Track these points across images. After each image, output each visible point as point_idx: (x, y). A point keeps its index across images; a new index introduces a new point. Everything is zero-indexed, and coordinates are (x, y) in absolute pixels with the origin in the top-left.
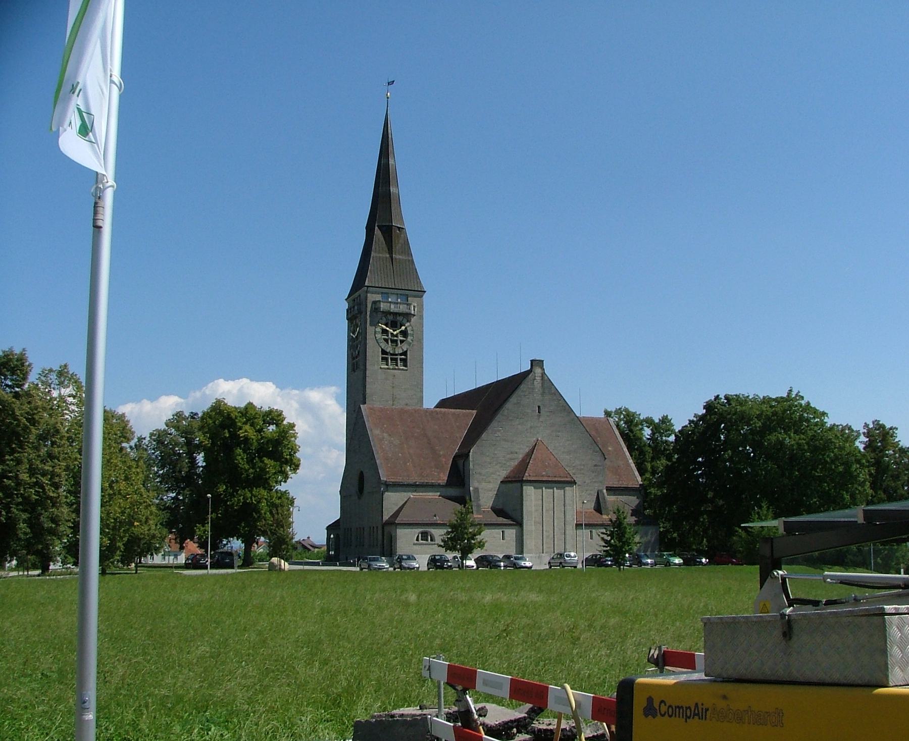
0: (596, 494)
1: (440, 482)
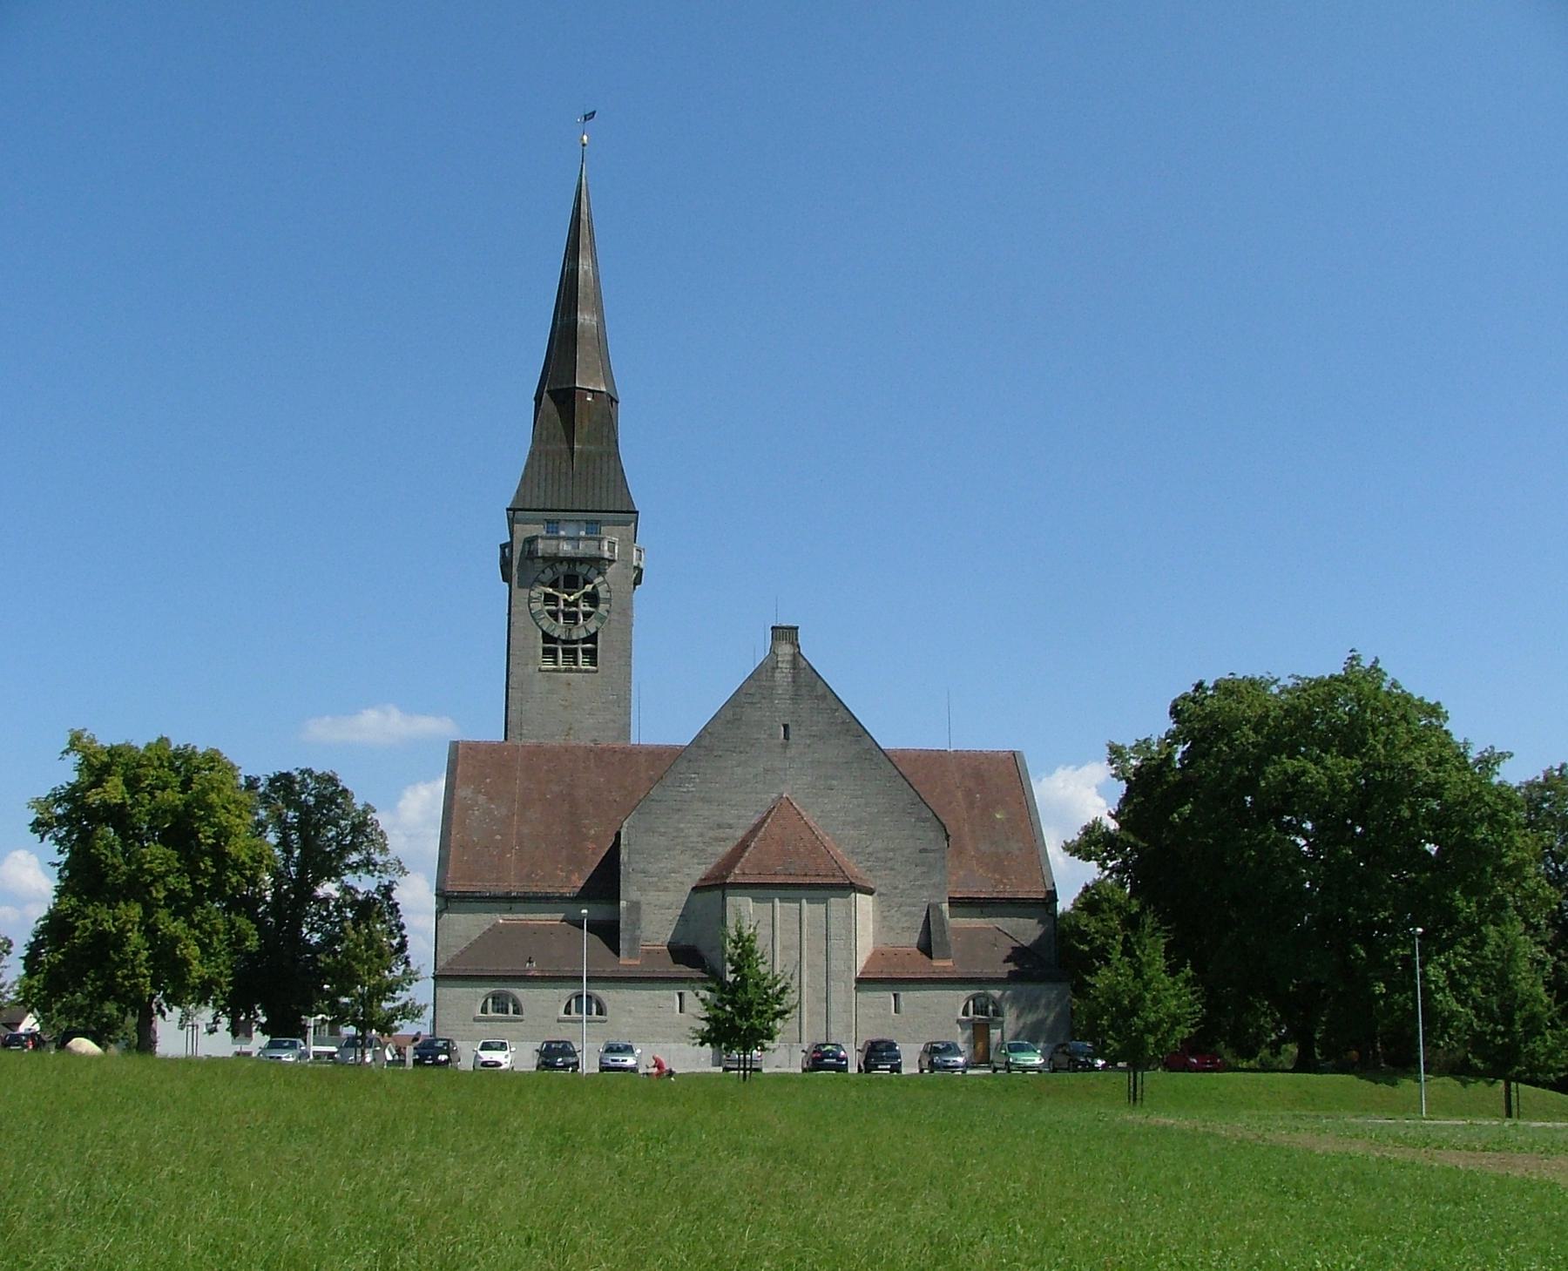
1: (565, 890)
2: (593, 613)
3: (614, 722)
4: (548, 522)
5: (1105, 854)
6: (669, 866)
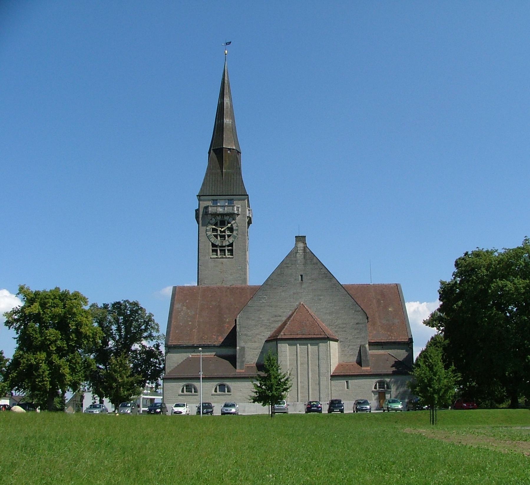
0: (359, 348)
2: (231, 235)
3: (240, 277)
4: (213, 200)
5: (439, 325)
6: (256, 332)
